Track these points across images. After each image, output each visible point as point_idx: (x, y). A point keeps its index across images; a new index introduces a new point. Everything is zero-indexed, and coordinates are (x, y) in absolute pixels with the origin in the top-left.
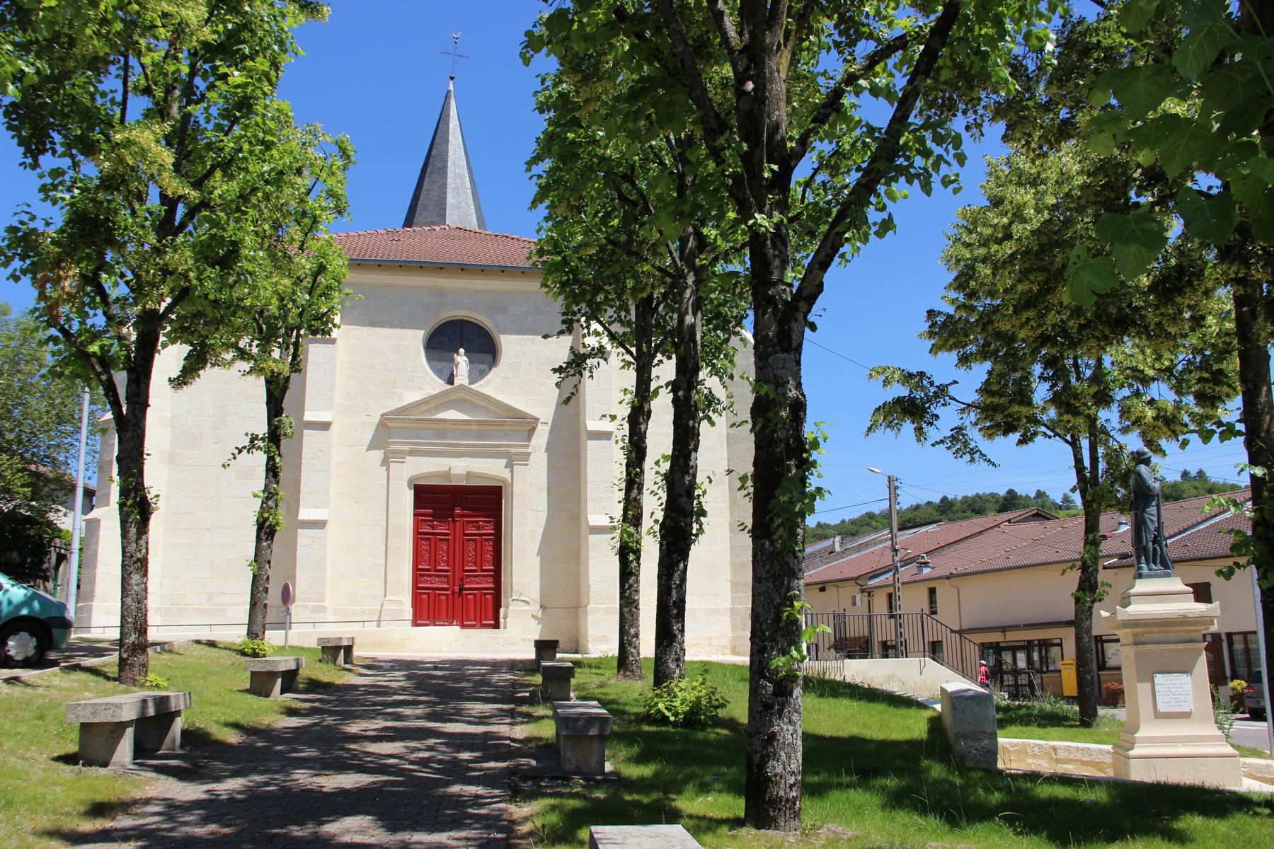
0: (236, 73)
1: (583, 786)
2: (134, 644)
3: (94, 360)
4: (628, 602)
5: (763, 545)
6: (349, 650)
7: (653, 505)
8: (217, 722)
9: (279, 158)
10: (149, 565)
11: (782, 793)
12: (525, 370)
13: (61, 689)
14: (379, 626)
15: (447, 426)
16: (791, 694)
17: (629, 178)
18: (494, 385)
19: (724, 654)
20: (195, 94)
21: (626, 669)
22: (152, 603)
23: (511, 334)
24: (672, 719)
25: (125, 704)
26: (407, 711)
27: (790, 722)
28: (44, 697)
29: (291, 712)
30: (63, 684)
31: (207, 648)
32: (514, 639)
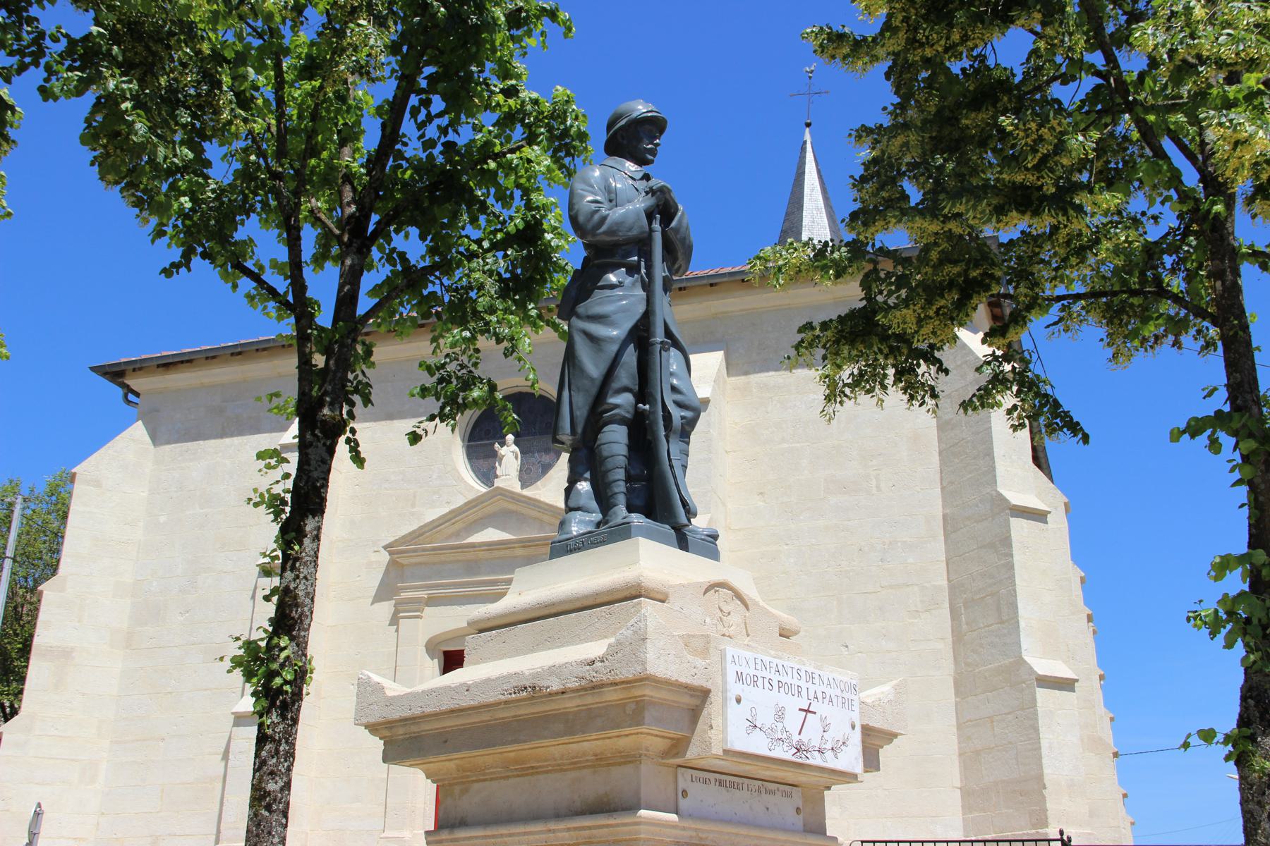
4: (476, 837)
15: (481, 555)
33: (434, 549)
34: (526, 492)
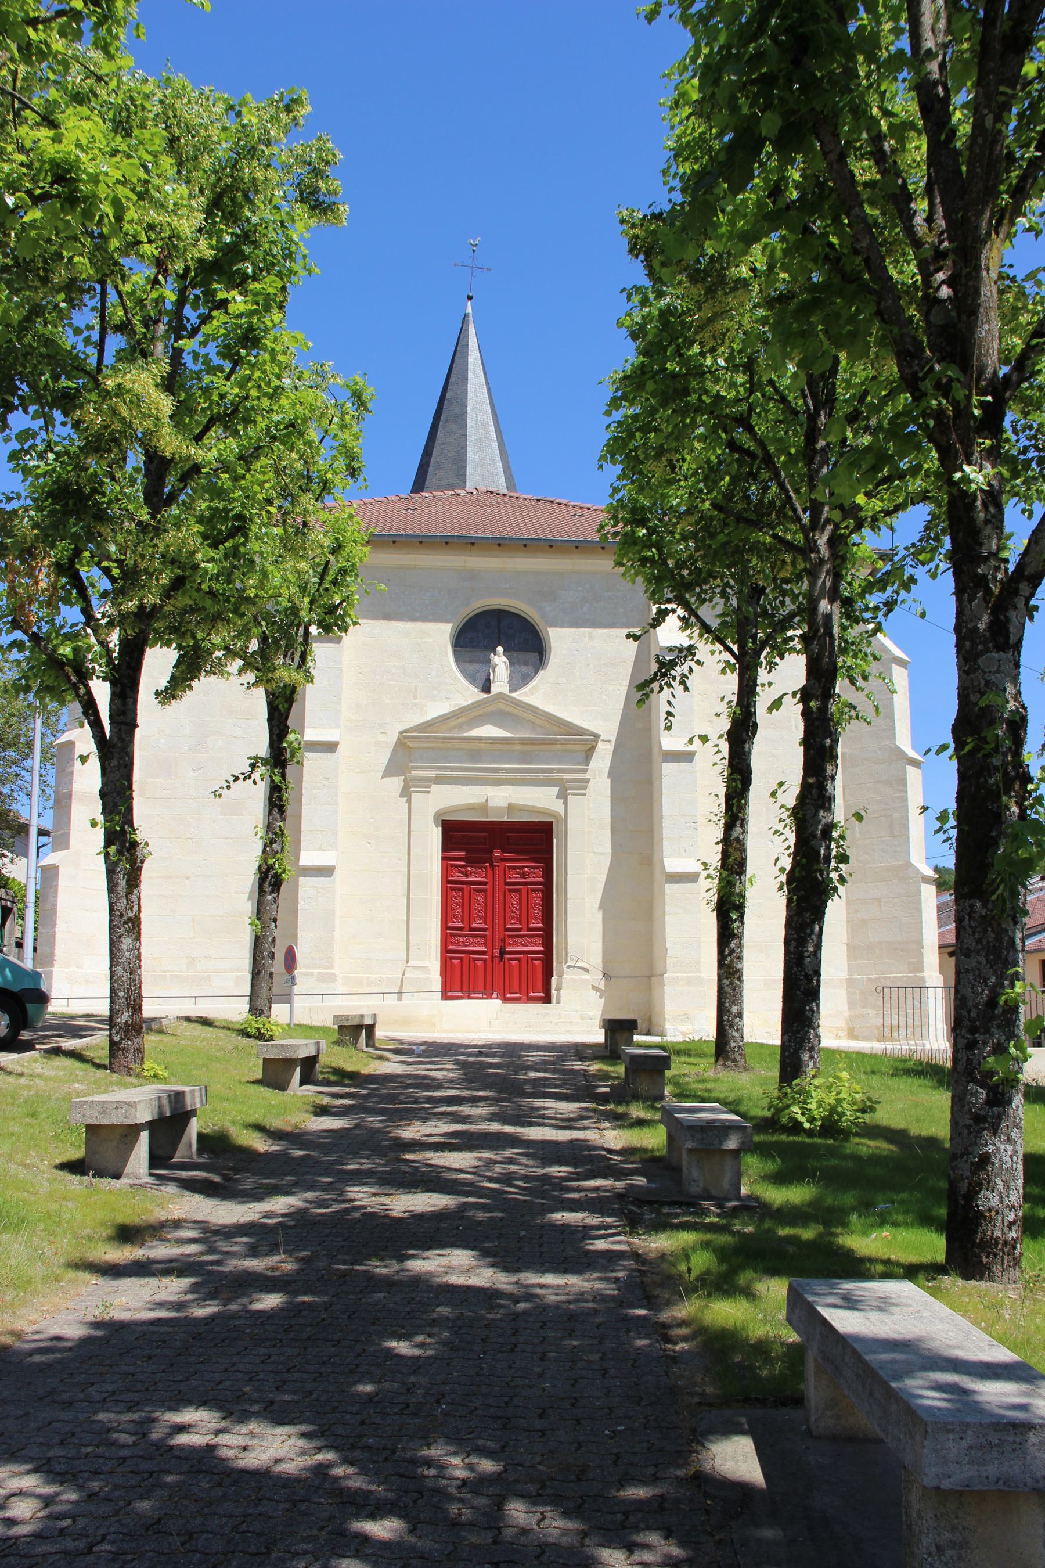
0: (239, 298)
1: (718, 1215)
2: (127, 1025)
3: (69, 669)
4: (729, 971)
5: (971, 906)
6: (371, 1029)
7: (769, 849)
8: (234, 1122)
9: (285, 409)
10: (142, 927)
11: (998, 1233)
12: (585, 674)
13: (47, 1079)
14: (400, 999)
15: (484, 746)
16: (1009, 1102)
17: (744, 422)
18: (541, 693)
19: (837, 1037)
20: (185, 329)
21: (727, 1058)
22: (147, 973)
23: (562, 626)
24: (807, 1125)
25: (138, 1100)
26: (465, 1110)
27: (1009, 1140)
28: (29, 1087)
29: (322, 1111)
30: (48, 1073)
31: (199, 1027)
32: (572, 1016)
33: (445, 738)
34: (514, 695)
